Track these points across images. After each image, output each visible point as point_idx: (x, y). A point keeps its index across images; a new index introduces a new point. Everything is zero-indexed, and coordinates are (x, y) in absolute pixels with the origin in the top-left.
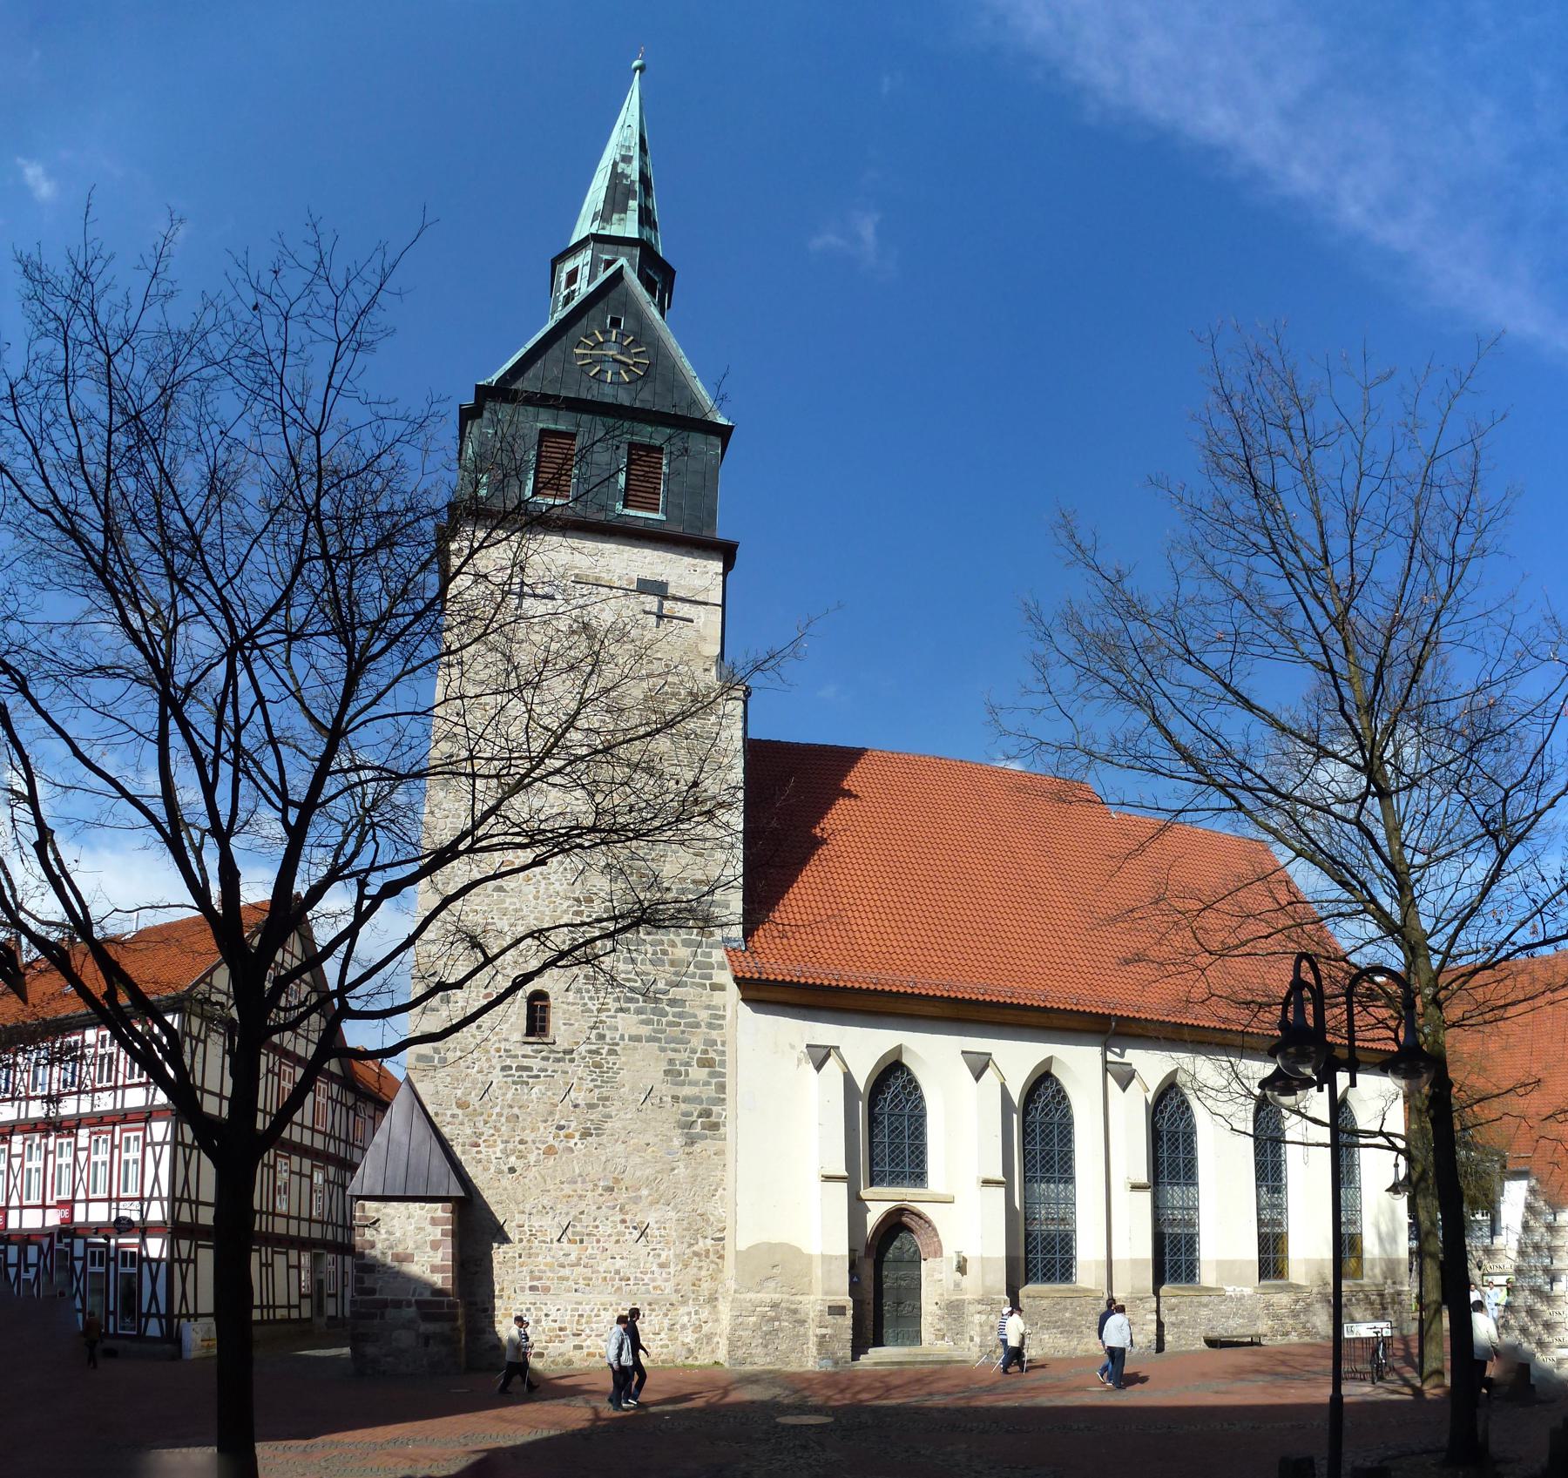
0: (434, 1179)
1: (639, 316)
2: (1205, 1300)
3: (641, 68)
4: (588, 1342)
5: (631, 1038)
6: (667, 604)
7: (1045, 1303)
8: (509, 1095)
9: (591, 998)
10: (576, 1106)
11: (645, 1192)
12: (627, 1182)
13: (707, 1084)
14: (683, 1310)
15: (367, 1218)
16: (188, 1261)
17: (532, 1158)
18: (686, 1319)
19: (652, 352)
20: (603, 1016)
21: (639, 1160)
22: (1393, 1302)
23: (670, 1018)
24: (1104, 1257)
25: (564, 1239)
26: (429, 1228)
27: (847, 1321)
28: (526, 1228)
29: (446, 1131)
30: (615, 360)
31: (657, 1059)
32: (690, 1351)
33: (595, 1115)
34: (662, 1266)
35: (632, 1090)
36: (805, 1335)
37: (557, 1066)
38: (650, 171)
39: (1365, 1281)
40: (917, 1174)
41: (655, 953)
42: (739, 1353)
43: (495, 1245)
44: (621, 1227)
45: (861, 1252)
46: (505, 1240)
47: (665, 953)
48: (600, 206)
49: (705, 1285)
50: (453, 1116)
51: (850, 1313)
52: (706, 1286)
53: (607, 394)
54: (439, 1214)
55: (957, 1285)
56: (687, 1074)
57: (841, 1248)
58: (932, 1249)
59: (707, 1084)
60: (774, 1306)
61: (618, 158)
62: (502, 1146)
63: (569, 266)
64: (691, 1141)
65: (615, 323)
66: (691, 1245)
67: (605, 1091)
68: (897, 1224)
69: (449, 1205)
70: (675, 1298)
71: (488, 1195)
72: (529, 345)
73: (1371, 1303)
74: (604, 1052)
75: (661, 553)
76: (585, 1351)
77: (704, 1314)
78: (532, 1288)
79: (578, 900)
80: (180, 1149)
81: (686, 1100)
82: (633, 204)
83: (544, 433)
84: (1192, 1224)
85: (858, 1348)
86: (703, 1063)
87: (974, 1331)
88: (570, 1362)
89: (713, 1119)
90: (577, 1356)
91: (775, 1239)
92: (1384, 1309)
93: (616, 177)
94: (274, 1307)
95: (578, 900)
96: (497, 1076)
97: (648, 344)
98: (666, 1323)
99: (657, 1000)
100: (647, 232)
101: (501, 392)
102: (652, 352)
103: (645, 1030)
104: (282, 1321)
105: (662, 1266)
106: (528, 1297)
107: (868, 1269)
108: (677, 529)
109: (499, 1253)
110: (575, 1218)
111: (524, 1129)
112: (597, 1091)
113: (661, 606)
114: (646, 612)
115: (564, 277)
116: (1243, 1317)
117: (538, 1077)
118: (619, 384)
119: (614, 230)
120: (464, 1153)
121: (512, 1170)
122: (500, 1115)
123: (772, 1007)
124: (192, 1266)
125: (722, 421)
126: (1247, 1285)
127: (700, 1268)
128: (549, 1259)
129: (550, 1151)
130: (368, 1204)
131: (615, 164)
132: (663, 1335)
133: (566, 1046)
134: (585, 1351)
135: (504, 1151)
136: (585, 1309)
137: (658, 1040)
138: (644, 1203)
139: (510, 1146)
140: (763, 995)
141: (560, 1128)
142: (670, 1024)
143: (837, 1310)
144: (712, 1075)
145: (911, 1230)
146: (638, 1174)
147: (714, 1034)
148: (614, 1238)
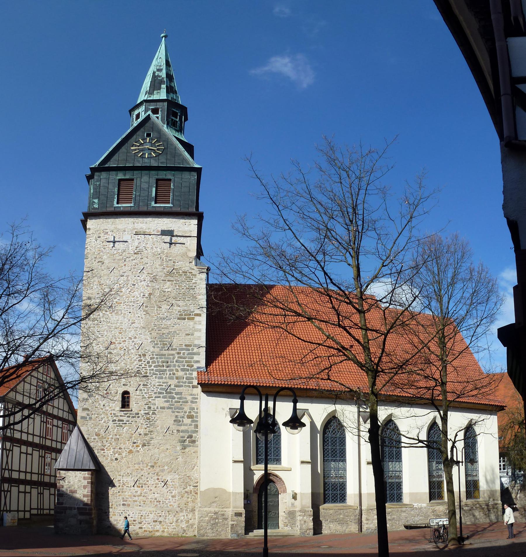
0: (85, 462)
1: (160, 132)
2: (404, 509)
3: (165, 37)
4: (144, 526)
5: (161, 408)
6: (174, 239)
7: (331, 511)
8: (115, 431)
9: (146, 393)
10: (140, 435)
11: (166, 468)
12: (159, 464)
13: (191, 425)
14: (181, 514)
15: (61, 477)
16: (7, 491)
17: (124, 455)
18: (182, 518)
19: (165, 144)
20: (150, 400)
21: (164, 455)
22: (494, 508)
23: (176, 399)
24: (357, 492)
25: (136, 486)
26: (83, 481)
27: (243, 519)
28: (121, 481)
29: (92, 445)
30: (149, 149)
31: (171, 416)
32: (185, 531)
33: (147, 438)
34: (173, 497)
35: (161, 428)
36: (227, 524)
37: (133, 419)
38: (173, 73)
39: (481, 499)
40: (278, 460)
41: (170, 374)
42: (202, 532)
43: (110, 488)
44: (157, 481)
45: (251, 491)
46: (114, 486)
47: (174, 374)
48: (148, 89)
49: (190, 505)
50: (94, 439)
51: (244, 515)
52: (190, 505)
53: (147, 163)
54: (87, 475)
55: (293, 504)
56: (183, 421)
57: (241, 489)
58: (282, 490)
59: (191, 425)
60: (216, 513)
61: (155, 70)
62: (113, 450)
63: (136, 112)
64: (184, 448)
65: (149, 135)
66: (184, 489)
67: (151, 429)
68: (267, 479)
69: (90, 472)
70: (178, 509)
71: (107, 469)
72: (110, 150)
73: (483, 509)
74: (151, 413)
75: (171, 219)
76: (143, 529)
77: (190, 516)
78: (123, 505)
79: (140, 355)
80: (5, 451)
81: (182, 431)
82: (164, 86)
83: (120, 180)
84: (400, 477)
85: (248, 529)
86: (189, 417)
87: (298, 523)
88: (137, 534)
89: (193, 439)
90: (140, 531)
91: (216, 487)
92: (489, 511)
93: (154, 76)
94: (43, 509)
95: (140, 355)
96: (111, 424)
97: (163, 141)
98: (175, 519)
99: (170, 393)
100: (171, 95)
101: (102, 168)
102: (165, 144)
103: (166, 405)
104: (46, 515)
105: (173, 497)
106: (122, 508)
107: (255, 498)
108: (178, 209)
109: (111, 491)
110: (140, 477)
111: (121, 444)
112: (148, 429)
113: (171, 240)
114: (165, 243)
115: (135, 116)
116: (422, 516)
117: (126, 423)
118: (151, 158)
119: (155, 97)
120: (98, 453)
121: (116, 459)
122: (112, 438)
123: (214, 394)
124: (9, 493)
125: (196, 166)
126: (424, 503)
127: (188, 498)
128: (130, 494)
129: (131, 452)
130: (61, 472)
131: (154, 73)
132: (173, 524)
133: (136, 412)
134: (143, 529)
135: (113, 452)
136: (143, 513)
137: (172, 408)
138: (166, 472)
139: (116, 450)
140: (211, 389)
141: (134, 443)
142: (176, 402)
143: (238, 514)
144: (193, 421)
145: (274, 482)
146: (164, 460)
147: (194, 405)
148: (154, 486)
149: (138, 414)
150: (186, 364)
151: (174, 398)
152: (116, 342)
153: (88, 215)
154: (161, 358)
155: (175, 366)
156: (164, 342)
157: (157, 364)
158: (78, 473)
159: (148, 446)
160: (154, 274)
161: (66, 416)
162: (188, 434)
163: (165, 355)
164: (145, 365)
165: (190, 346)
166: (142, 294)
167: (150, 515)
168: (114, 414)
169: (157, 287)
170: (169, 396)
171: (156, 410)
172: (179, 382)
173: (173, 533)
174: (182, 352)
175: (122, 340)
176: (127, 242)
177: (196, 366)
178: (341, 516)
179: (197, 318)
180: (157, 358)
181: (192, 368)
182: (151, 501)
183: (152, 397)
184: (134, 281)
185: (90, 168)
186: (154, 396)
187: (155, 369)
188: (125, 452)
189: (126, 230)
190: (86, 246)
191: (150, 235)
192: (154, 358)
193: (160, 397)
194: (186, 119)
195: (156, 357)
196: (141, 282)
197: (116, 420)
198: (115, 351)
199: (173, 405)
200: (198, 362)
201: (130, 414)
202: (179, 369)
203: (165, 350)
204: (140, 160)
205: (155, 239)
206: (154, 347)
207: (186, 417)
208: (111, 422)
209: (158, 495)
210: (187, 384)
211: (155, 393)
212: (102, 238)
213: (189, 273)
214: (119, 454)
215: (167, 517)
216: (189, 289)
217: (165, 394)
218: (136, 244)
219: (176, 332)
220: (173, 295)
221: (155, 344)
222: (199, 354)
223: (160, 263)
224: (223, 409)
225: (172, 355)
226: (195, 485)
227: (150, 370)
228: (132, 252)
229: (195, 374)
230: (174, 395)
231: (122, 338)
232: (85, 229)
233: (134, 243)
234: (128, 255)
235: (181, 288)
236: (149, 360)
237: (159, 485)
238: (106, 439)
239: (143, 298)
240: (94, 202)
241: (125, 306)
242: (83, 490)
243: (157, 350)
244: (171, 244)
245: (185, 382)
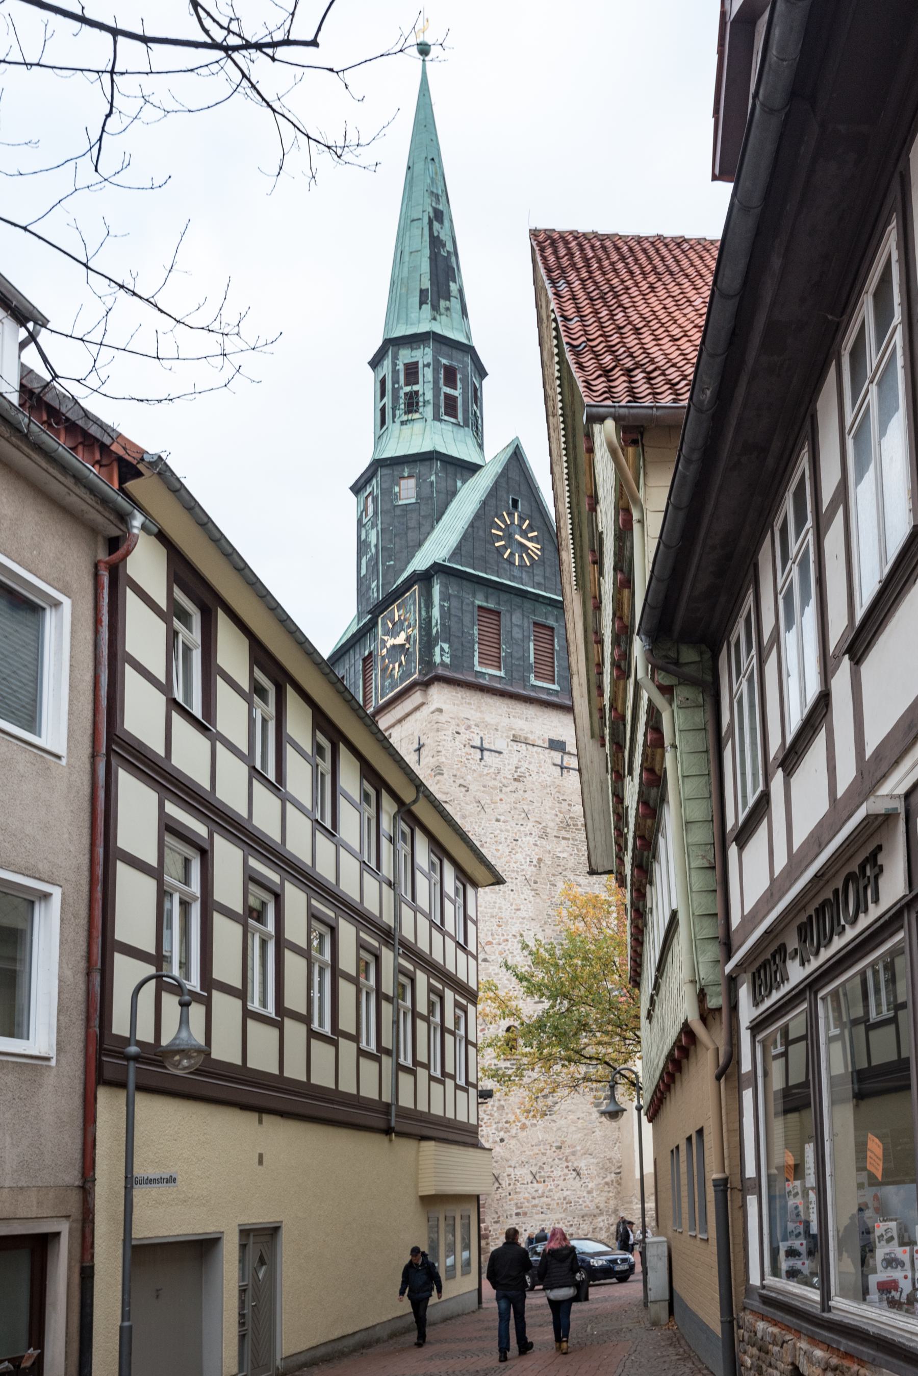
11: (578, 1148)
14: (600, 1219)
21: (574, 1129)
28: (513, 1176)
44: (566, 1171)
62: (495, 1126)
78: (517, 1214)
105: (589, 1192)
111: (507, 1114)
139: (500, 1125)
146: (575, 1136)
148: (562, 1178)
152: (494, 942)
160: (544, 824)
166: (528, 860)
169: (549, 848)
182: (558, 1204)
191: (533, 745)
196: (526, 835)
204: (506, 566)
205: (541, 756)
209: (568, 1193)
212: (464, 737)
218: (514, 761)
220: (570, 864)
223: (550, 805)
226: (618, 1171)
228: (510, 777)
231: (503, 935)
233: (513, 757)
237: (570, 1176)
239: (530, 865)
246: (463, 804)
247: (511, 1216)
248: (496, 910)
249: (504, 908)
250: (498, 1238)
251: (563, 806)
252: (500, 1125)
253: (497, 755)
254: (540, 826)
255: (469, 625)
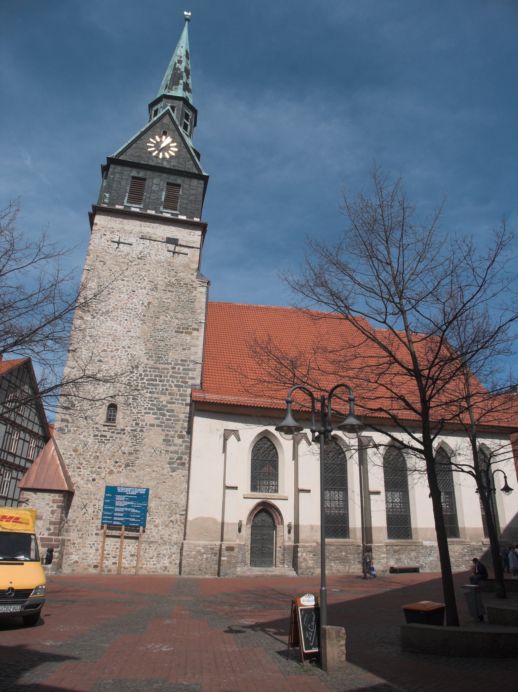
6: (178, 249)
8: (96, 447)
9: (134, 408)
10: (124, 453)
21: (150, 478)
23: (167, 417)
26: (51, 504)
28: (97, 506)
33: (132, 458)
37: (117, 436)
56: (173, 441)
60: (204, 547)
62: (90, 470)
63: (155, 108)
66: (169, 517)
67: (137, 447)
79: (132, 367)
81: (172, 452)
93: (176, 69)
103: (157, 422)
111: (100, 462)
112: (134, 447)
117: (109, 440)
121: (94, 480)
122: (91, 456)
131: (175, 64)
132: (154, 559)
133: (122, 427)
139: (94, 469)
141: (116, 462)
149: (124, 430)
150: (181, 380)
151: (165, 415)
152: (108, 350)
153: (97, 210)
154: (154, 372)
155: (168, 381)
156: (157, 354)
157: (149, 377)
158: (46, 495)
159: (132, 466)
160: (156, 283)
161: (36, 429)
162: (177, 456)
163: (158, 369)
164: (137, 377)
165: (185, 361)
166: (141, 302)
167: (127, 547)
168: (97, 428)
170: (160, 413)
171: (144, 427)
172: (171, 399)
173: (154, 570)
174: (177, 367)
175: (115, 348)
176: (131, 245)
177: (190, 382)
178: (343, 554)
179: (195, 333)
180: (150, 371)
181: (187, 385)
183: (141, 413)
184: (134, 288)
185: (108, 158)
186: (143, 411)
187: (147, 382)
188: (105, 472)
189: (133, 232)
190: (90, 242)
191: (155, 241)
192: (147, 371)
193: (150, 413)
194: (195, 125)
195: (149, 369)
196: (141, 289)
197: (97, 436)
198: (106, 359)
199: (164, 423)
200: (193, 378)
201: (115, 429)
202: (173, 385)
203: (159, 364)
205: (160, 246)
206: (148, 359)
207: (176, 436)
208: (92, 437)
210: (180, 401)
211: (145, 409)
213: (190, 285)
214: (97, 475)
215: (147, 551)
216: (188, 301)
217: (155, 411)
218: (141, 248)
219: (172, 345)
221: (149, 356)
222: (194, 370)
224: (218, 430)
225: (167, 369)
227: (142, 383)
229: (189, 391)
230: (165, 412)
231: (115, 346)
232: (92, 224)
233: (139, 247)
234: (131, 259)
235: (181, 300)
236: (141, 372)
238: (84, 456)
239: (141, 306)
240: (105, 196)
241: (122, 313)
242: (51, 516)
243: (151, 362)
244: (174, 253)
245: (178, 400)
246: (100, 271)
247: (92, 534)
248: (113, 331)
249: (119, 330)
250: (80, 550)
251: (171, 273)
252: (94, 469)
253: (129, 246)
254: (153, 284)
255: (125, 185)
